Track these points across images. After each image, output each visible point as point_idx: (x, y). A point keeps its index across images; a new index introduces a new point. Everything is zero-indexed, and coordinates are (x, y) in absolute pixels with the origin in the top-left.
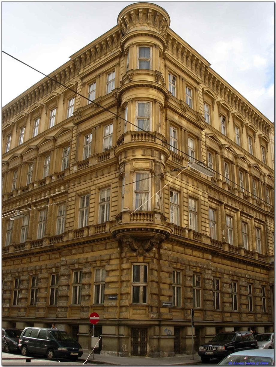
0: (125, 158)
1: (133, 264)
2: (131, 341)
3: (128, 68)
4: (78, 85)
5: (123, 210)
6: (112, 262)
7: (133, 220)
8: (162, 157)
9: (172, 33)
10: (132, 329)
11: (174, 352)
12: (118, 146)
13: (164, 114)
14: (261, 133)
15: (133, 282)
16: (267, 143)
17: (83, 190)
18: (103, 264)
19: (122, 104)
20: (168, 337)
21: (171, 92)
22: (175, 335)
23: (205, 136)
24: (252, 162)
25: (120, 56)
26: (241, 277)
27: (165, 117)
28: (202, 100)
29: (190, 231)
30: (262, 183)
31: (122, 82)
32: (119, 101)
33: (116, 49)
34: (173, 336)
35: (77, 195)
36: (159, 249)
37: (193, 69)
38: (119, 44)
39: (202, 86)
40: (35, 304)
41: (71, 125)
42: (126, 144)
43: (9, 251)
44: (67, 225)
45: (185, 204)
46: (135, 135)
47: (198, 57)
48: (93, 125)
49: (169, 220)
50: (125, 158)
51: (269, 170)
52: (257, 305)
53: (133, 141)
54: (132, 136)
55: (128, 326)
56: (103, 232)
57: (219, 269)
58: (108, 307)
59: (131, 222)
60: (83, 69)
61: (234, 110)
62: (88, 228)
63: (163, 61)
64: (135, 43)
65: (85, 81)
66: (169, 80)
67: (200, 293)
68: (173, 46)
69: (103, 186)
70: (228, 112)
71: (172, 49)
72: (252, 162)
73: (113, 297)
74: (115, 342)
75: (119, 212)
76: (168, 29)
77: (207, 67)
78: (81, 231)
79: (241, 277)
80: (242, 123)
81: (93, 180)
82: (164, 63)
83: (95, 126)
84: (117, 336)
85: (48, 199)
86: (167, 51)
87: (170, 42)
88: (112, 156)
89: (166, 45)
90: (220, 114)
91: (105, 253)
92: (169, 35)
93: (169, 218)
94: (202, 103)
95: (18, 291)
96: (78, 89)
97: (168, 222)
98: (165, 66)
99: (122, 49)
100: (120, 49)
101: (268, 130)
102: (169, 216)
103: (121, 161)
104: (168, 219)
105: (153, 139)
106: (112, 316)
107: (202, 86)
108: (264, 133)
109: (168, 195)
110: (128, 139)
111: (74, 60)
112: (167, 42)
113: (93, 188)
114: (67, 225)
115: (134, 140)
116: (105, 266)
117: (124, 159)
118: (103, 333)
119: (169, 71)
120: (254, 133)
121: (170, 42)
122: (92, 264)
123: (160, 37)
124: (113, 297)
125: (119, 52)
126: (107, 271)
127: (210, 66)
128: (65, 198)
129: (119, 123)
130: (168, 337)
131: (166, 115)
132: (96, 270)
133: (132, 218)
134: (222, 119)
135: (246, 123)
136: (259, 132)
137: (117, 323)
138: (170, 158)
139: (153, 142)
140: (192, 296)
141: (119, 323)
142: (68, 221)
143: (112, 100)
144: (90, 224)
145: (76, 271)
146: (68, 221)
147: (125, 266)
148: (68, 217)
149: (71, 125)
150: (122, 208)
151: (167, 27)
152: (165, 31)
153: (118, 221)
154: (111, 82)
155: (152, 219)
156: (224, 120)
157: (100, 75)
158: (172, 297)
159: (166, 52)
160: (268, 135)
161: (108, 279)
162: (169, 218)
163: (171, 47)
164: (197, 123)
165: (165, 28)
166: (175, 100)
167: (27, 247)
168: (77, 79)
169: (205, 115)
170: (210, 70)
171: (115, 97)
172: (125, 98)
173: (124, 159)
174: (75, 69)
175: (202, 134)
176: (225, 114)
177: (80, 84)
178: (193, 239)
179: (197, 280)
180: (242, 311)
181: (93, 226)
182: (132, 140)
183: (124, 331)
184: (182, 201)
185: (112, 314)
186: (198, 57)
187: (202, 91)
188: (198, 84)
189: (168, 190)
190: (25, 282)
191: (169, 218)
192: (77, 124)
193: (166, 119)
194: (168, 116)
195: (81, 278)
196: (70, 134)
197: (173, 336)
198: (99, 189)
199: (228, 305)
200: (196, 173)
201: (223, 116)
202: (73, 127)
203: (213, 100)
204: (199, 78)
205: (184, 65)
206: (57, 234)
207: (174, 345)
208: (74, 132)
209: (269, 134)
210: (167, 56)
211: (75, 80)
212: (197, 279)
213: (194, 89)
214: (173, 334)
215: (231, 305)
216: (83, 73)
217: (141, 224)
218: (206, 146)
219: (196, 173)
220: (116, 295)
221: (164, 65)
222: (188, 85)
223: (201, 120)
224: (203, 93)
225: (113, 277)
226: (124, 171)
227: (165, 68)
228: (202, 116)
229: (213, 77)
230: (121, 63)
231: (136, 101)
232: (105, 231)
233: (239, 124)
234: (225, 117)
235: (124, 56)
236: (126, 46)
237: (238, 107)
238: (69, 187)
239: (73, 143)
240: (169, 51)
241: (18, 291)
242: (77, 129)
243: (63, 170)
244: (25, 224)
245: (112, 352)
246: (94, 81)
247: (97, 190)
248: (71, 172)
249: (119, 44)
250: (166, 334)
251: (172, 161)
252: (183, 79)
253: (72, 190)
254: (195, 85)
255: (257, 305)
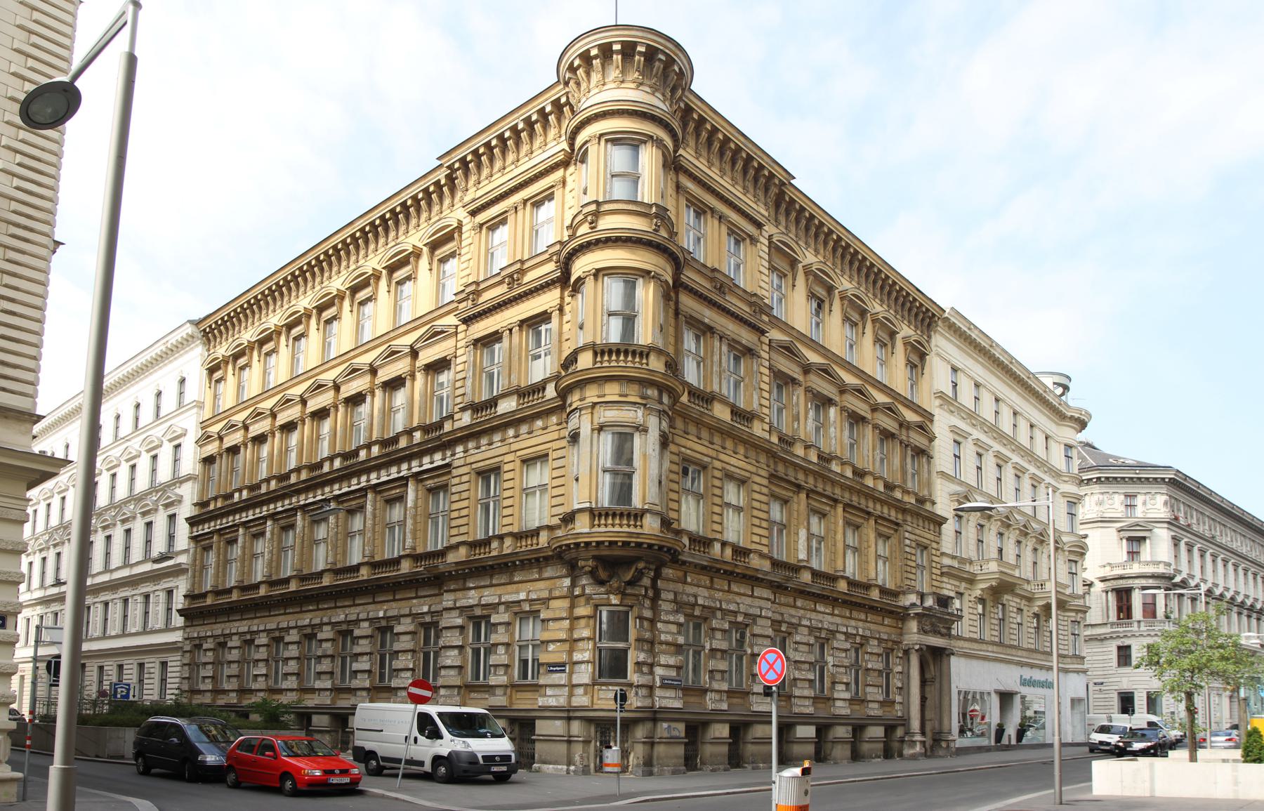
0: (581, 400)
1: (599, 608)
2: (596, 746)
3: (585, 193)
4: (464, 229)
5: (577, 507)
6: (554, 604)
7: (599, 526)
8: (665, 399)
9: (699, 103)
10: (597, 725)
11: (684, 768)
12: (563, 373)
13: (672, 304)
14: (911, 332)
15: (600, 640)
16: (922, 356)
17: (488, 462)
18: (536, 607)
19: (573, 279)
20: (671, 741)
21: (691, 250)
22: (686, 737)
23: (769, 345)
24: (881, 398)
25: (565, 164)
26: (837, 632)
27: (673, 307)
28: (766, 264)
29: (724, 544)
30: (901, 443)
31: (573, 227)
32: (566, 273)
33: (555, 143)
34: (682, 738)
35: (472, 472)
36: (658, 576)
37: (748, 191)
38: (563, 131)
39: (769, 229)
40: (350, 682)
41: (451, 320)
42: (582, 371)
43: (323, 580)
44: (454, 532)
45: (717, 492)
46: (603, 353)
47: (762, 159)
48: (505, 324)
49: (679, 524)
50: (581, 400)
51: (922, 415)
52: (837, 683)
53: (598, 365)
54: (595, 354)
55: (589, 720)
56: (534, 547)
57: (645, 648)
58: (546, 686)
59: (594, 530)
60: (475, 189)
61: (845, 284)
62: (501, 538)
63: (672, 174)
64: (601, 135)
65: (483, 217)
66: (686, 221)
67: (744, 662)
68: (698, 136)
69: (533, 455)
70: (830, 289)
71: (697, 143)
72: (881, 398)
73: (558, 669)
74: (563, 748)
75: (566, 509)
76: (687, 93)
77: (784, 184)
78: (485, 545)
79: (837, 632)
80: (863, 313)
81: (508, 441)
82: (675, 180)
83: (509, 327)
84: (566, 738)
85: (406, 479)
86: (684, 149)
87: (692, 126)
88: (550, 392)
89: (680, 136)
90: (812, 295)
91: (539, 590)
92: (688, 110)
93: (678, 520)
94: (766, 272)
95: (432, 653)
96: (464, 244)
97: (677, 527)
98: (678, 187)
99: (572, 145)
100: (565, 146)
101: (929, 325)
102: (679, 515)
103: (570, 405)
104: (676, 523)
105: (644, 361)
106: (552, 702)
107: (769, 229)
108: (919, 332)
109: (678, 474)
110: (585, 360)
111: (450, 165)
112: (684, 126)
113: (508, 458)
114: (454, 532)
115: (601, 362)
116: (539, 611)
117: (579, 403)
118: (536, 733)
119: (687, 200)
120: (892, 334)
121: (692, 126)
122: (511, 607)
123: (667, 118)
124: (558, 669)
125: (563, 153)
126: (543, 621)
127: (792, 181)
128: (445, 478)
129: (567, 340)
130: (671, 741)
131: (677, 303)
132: (521, 619)
133: (596, 522)
134: (815, 305)
135: (873, 312)
136: (906, 331)
137: (565, 715)
138: (684, 399)
139: (644, 366)
140: (813, 678)
141: (568, 714)
142: (454, 523)
143: (551, 266)
144: (505, 531)
145: (477, 621)
146: (454, 523)
147: (582, 611)
148: (455, 515)
149: (451, 320)
150: (575, 502)
151: (683, 90)
152: (680, 98)
153: (566, 527)
154: (546, 225)
155: (638, 523)
156: (819, 306)
157: (516, 208)
158: (726, 671)
159: (681, 152)
160: (929, 337)
161: (546, 636)
162: (678, 520)
163: (694, 137)
164: (752, 320)
165: (680, 91)
166: (703, 270)
167: (364, 573)
168: (460, 214)
169: (772, 298)
170: (793, 190)
171: (556, 263)
172: (580, 266)
173: (579, 403)
174: (453, 190)
175: (762, 343)
176: (821, 292)
177: (469, 226)
178: (730, 561)
179: (738, 637)
180: (836, 695)
181: (511, 534)
182: (595, 363)
183: (576, 727)
184: (710, 485)
185: (553, 699)
186: (762, 159)
187: (766, 242)
188: (759, 226)
189: (678, 464)
190: (501, 650)
191: (678, 520)
192: (467, 321)
193: (677, 313)
194: (681, 306)
195: (488, 633)
196: (450, 343)
197: (682, 738)
198: (524, 461)
199: (842, 687)
200: (743, 428)
201: (819, 298)
202: (457, 326)
203: (793, 263)
204: (760, 210)
205: (725, 183)
206: (430, 548)
207: (685, 754)
208: (460, 336)
209: (932, 333)
210: (684, 163)
211: (453, 213)
212: (738, 635)
213: (748, 240)
214: (683, 735)
215: (880, 689)
216: (474, 200)
217: (616, 534)
218: (770, 369)
219: (743, 428)
220: (563, 665)
221: (674, 185)
222: (733, 231)
223: (762, 311)
224: (769, 247)
225: (559, 630)
226: (579, 428)
227: (677, 192)
228: (766, 301)
229: (797, 207)
230: (569, 180)
231: (604, 275)
232: (538, 544)
233: (856, 314)
234: (823, 301)
235: (575, 164)
236: (580, 140)
237: (856, 276)
238: (453, 455)
239: (459, 360)
240: (687, 149)
241: (432, 653)
242: (466, 331)
243: (438, 420)
244: (355, 529)
245: (555, 766)
246: (501, 220)
247: (518, 462)
248: (458, 425)
249: (563, 131)
250: (669, 736)
251: (689, 404)
252: (720, 217)
253: (461, 462)
254: (750, 229)
255: (837, 683)
